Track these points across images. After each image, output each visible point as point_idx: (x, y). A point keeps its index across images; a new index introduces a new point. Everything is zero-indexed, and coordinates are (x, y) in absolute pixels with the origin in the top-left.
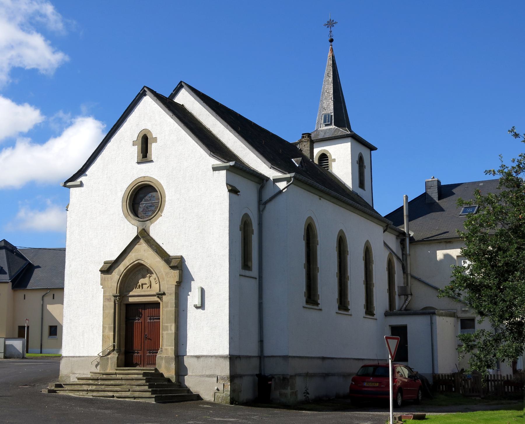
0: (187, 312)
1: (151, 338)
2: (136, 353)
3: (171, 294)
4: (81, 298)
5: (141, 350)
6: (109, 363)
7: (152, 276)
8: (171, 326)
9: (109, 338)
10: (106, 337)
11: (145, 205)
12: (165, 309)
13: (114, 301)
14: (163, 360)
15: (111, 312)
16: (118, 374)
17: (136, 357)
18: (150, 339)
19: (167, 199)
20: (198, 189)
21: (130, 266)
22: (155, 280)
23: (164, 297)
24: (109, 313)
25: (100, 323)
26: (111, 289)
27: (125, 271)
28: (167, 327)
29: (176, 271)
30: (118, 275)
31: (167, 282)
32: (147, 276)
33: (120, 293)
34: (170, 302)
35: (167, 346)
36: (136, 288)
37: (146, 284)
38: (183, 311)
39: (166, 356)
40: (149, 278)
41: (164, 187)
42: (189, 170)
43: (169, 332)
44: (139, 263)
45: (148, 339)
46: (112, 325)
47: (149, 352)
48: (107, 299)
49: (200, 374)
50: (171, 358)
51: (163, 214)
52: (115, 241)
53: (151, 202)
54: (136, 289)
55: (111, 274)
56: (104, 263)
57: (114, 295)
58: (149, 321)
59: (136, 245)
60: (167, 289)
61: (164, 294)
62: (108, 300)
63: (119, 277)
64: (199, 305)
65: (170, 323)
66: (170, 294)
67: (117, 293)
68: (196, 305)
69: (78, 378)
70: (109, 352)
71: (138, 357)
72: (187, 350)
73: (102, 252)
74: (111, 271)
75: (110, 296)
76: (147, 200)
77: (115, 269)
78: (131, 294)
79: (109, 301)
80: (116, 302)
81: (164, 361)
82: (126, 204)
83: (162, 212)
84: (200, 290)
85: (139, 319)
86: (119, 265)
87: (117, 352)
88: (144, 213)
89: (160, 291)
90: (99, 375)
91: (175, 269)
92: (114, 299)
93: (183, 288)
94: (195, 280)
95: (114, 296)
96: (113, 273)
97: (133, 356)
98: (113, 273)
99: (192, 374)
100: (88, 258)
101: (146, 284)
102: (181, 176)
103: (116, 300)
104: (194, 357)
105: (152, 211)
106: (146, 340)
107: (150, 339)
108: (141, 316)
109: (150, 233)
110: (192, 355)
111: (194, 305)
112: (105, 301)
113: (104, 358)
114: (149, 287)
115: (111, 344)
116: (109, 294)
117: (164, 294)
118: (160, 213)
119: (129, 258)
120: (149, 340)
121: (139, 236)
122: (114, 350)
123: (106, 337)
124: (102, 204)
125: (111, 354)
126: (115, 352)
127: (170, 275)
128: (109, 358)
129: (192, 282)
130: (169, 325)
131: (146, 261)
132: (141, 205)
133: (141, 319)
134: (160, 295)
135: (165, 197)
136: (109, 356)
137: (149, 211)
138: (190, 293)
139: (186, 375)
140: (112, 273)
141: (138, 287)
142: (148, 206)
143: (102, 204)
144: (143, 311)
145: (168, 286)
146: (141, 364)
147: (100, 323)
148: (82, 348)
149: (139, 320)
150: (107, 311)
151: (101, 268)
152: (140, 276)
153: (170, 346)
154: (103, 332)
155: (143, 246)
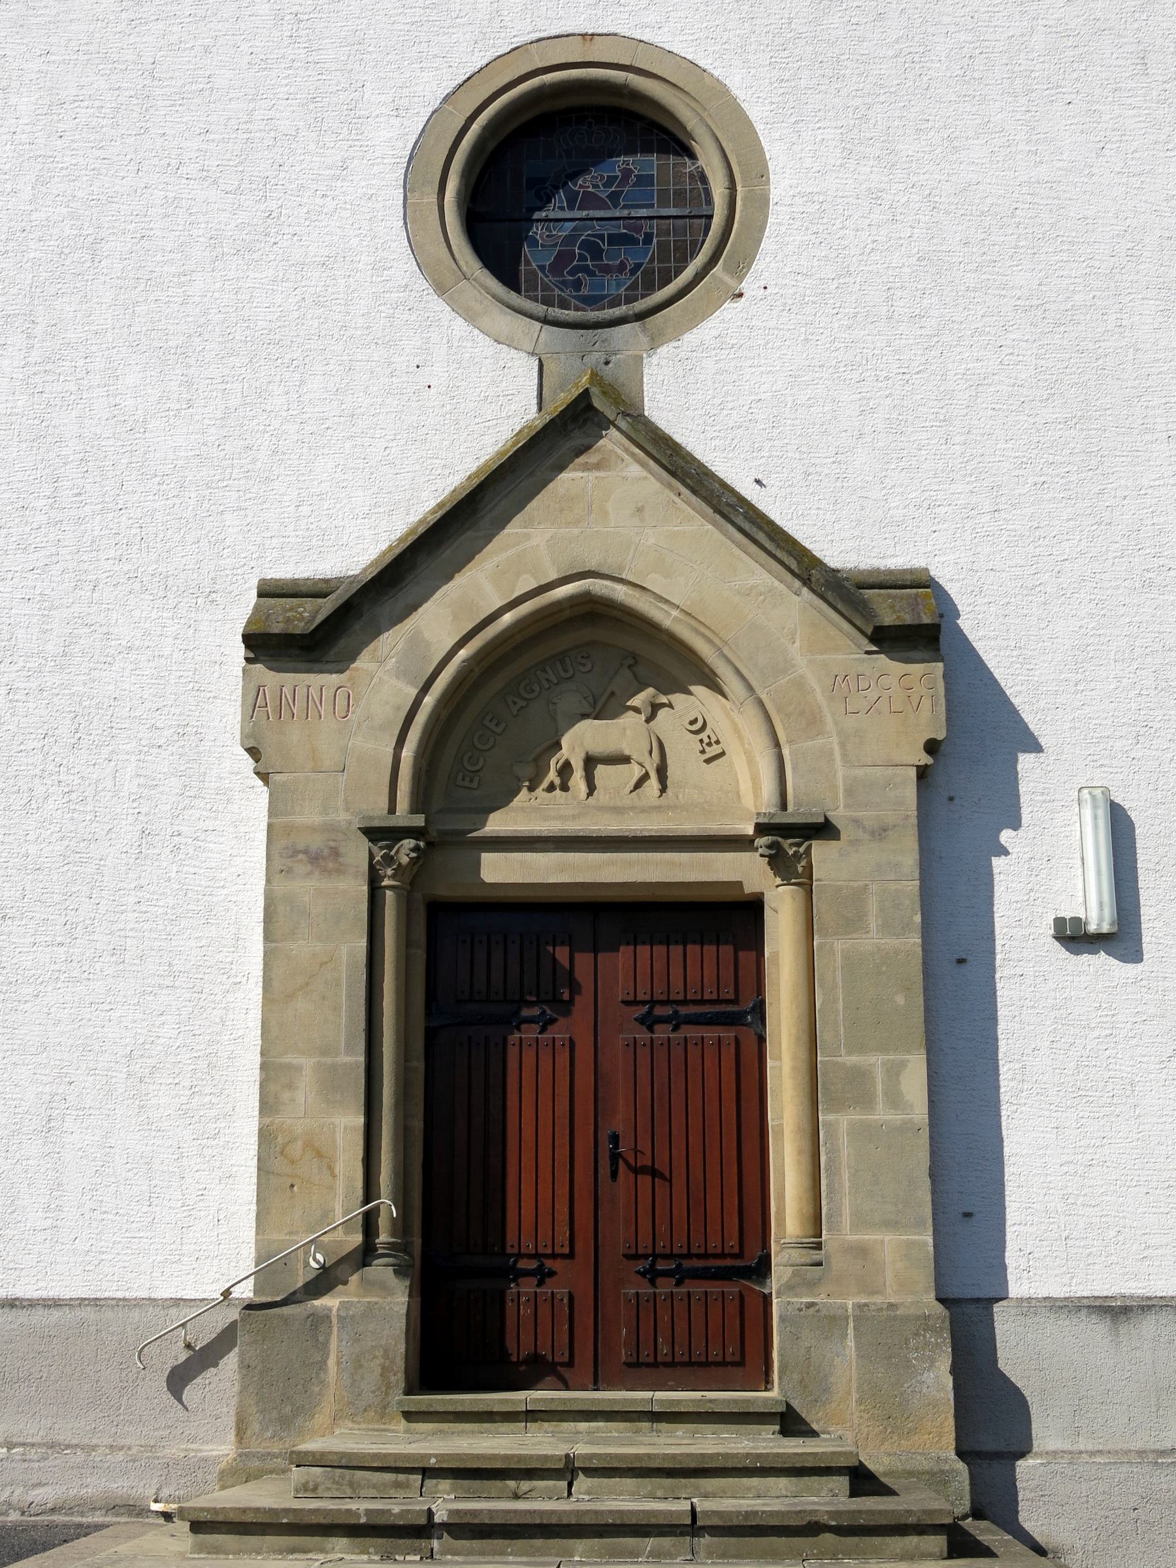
0: (994, 971)
1: (661, 1165)
2: (527, 1273)
3: (881, 833)
4: (32, 849)
5: (571, 1255)
6: (331, 1362)
7: (670, 706)
8: (894, 1071)
9: (319, 1155)
10: (296, 1149)
11: (574, 229)
12: (839, 945)
13: (372, 867)
14: (844, 1336)
15: (345, 958)
16: (590, 1472)
17: (526, 1311)
18: (654, 1173)
19: (779, 188)
20: (1029, 142)
21: (508, 618)
22: (704, 736)
23: (820, 850)
24: (322, 964)
25: (210, 1043)
26: (342, 779)
27: (463, 654)
28: (860, 1077)
29: (917, 669)
30: (402, 673)
31: (842, 745)
32: (637, 701)
33: (419, 803)
34: (874, 887)
35: (861, 1222)
36: (531, 789)
37: (626, 760)
38: (961, 961)
39: (860, 1307)
40: (648, 721)
41: (756, 113)
42: (946, 19)
43: (882, 1114)
44: (586, 600)
45: (636, 1171)
46: (349, 1050)
47: (643, 1274)
48: (306, 852)
49: (1139, 1445)
50: (918, 1318)
51: (748, 285)
52: (348, 445)
53: (625, 213)
54: (539, 791)
55: (341, 672)
56: (261, 595)
57: (376, 823)
58: (643, 1035)
59: (561, 468)
60: (849, 792)
61: (824, 830)
62: (315, 859)
63: (413, 692)
64: (1101, 919)
65: (883, 1048)
66: (873, 833)
67: (392, 810)
68: (1076, 921)
69: (194, 1516)
70: (323, 1267)
71: (544, 1311)
72: (1012, 1258)
73: (228, 516)
74: (342, 643)
75: (330, 828)
76: (590, 201)
77: (378, 633)
78: (497, 824)
79: (324, 870)
80: (386, 882)
81: (851, 1342)
82: (434, 199)
83: (740, 269)
84: (1103, 813)
85: (553, 1021)
86: (415, 607)
87: (399, 1272)
88: (564, 283)
89: (784, 806)
90: (389, 1477)
91: (912, 654)
92: (371, 856)
93: (951, 799)
94: (1042, 741)
95: (373, 834)
96: (356, 664)
97: (502, 1294)
98: (363, 663)
99: (1067, 1446)
100: (103, 556)
101: (626, 760)
102: (891, 53)
103: (388, 860)
104: (1079, 1309)
105: (633, 272)
106: (614, 1175)
107: (654, 1173)
108: (566, 997)
109: (647, 404)
110: (1056, 1294)
111: (1059, 922)
112: (287, 872)
113: (286, 1320)
114: (653, 783)
115: (339, 1210)
116: (316, 819)
117: (824, 830)
118: (727, 279)
119: (497, 559)
120: (645, 1181)
121: (590, 407)
122: (366, 1254)
123: (296, 1149)
124: (238, 191)
125: (345, 1283)
126: (381, 1270)
127: (873, 694)
128: (328, 1317)
129: (1025, 761)
130: (876, 1061)
131: (654, 582)
132: (538, 231)
133: (562, 1022)
134: (786, 837)
135: (763, 175)
136: (329, 1302)
137: (607, 270)
138: (1006, 836)
139: (1022, 1455)
140: (353, 658)
141: (552, 776)
142: (601, 237)
143: (238, 191)
144: (584, 961)
145: (859, 772)
146: (570, 1364)
147: (210, 1043)
148: (40, 1237)
149: (547, 1023)
150: (303, 948)
151: (249, 623)
152: (569, 700)
153: (890, 1225)
154: (267, 1105)
155: (625, 478)
